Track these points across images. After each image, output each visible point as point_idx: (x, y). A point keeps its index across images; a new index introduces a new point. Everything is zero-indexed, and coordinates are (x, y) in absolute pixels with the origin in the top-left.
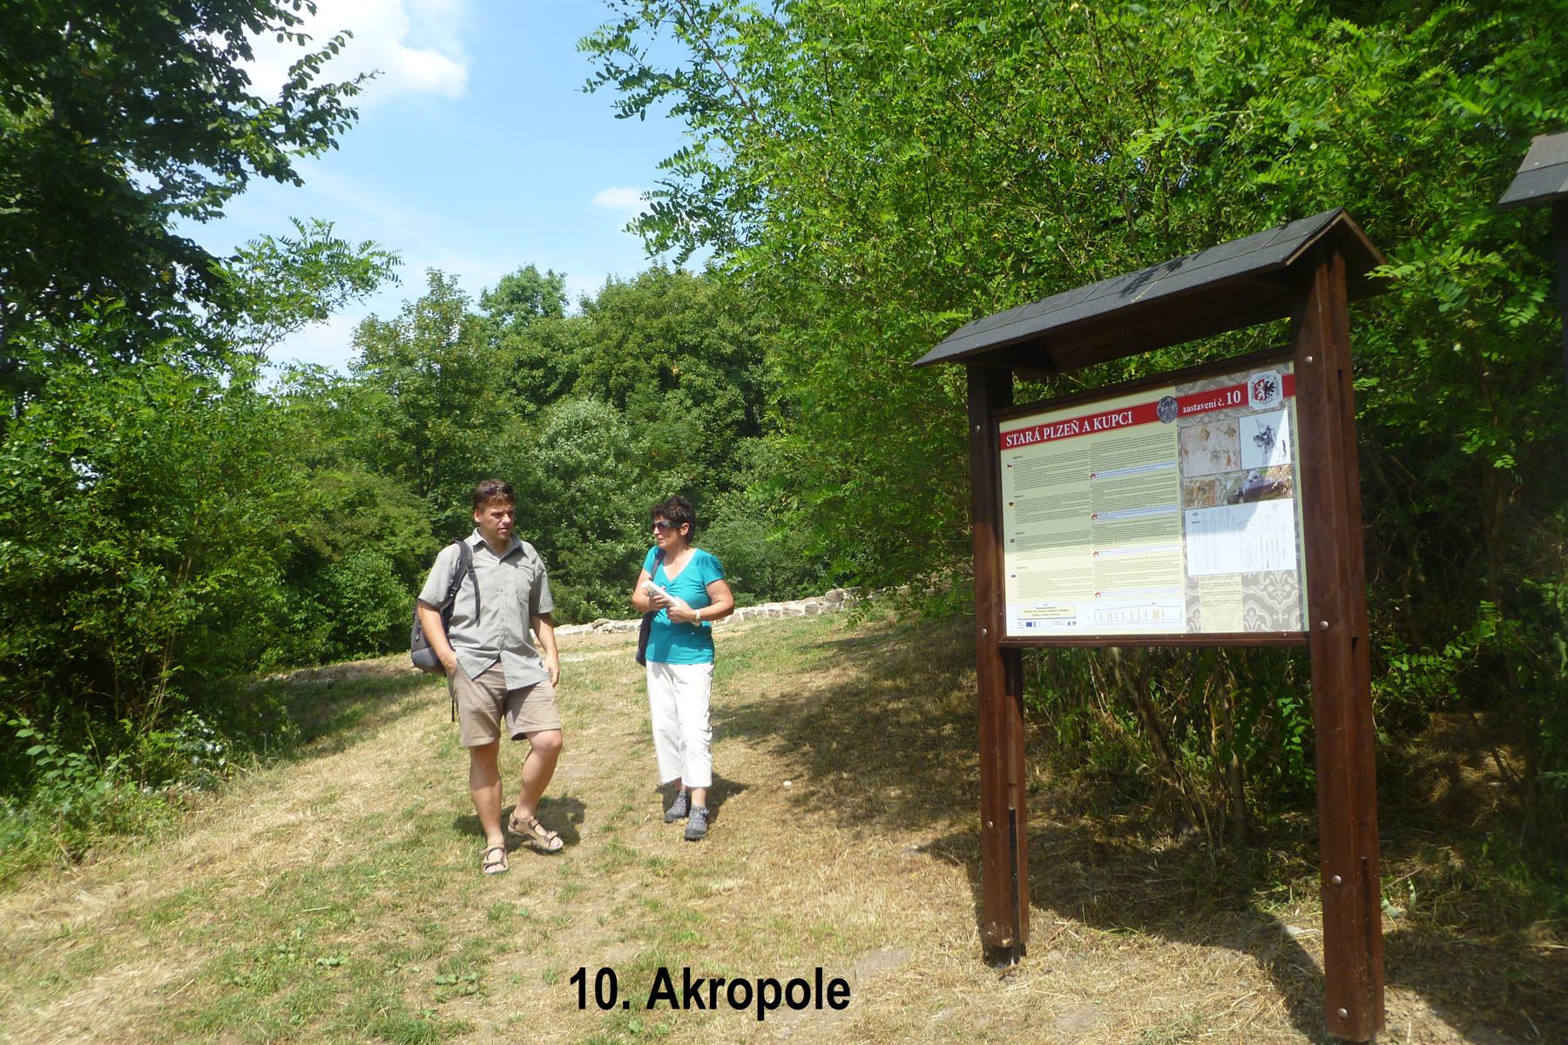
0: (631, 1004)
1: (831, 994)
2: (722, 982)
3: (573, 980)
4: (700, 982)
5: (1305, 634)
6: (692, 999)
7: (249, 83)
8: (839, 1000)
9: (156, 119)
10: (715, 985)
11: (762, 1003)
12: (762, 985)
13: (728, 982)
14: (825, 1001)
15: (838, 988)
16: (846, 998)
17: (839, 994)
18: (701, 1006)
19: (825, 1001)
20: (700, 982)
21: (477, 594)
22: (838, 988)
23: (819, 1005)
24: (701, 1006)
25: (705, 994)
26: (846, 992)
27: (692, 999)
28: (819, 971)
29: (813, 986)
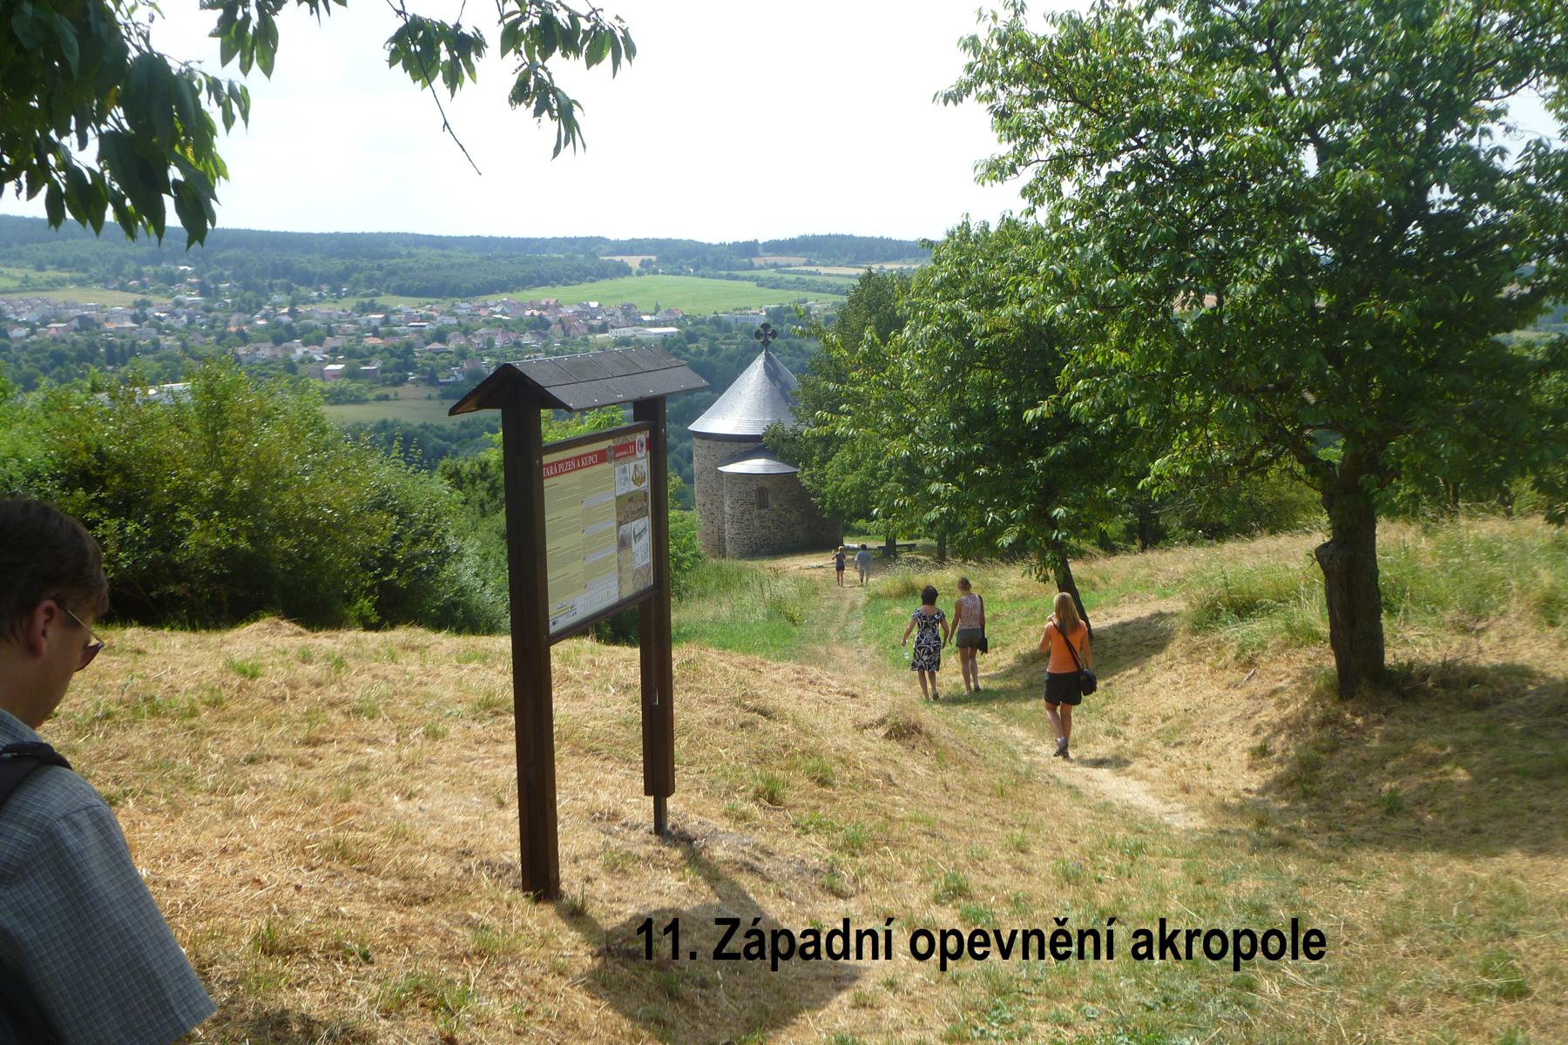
0: (699, 953)
1: (1307, 944)
2: (1198, 932)
3: (666, 931)
4: (1175, 933)
5: (541, 442)
6: (1168, 951)
7: (268, 69)
8: (979, 951)
9: (1333, 62)
10: (1190, 936)
11: (945, 954)
12: (1237, 935)
13: (1204, 933)
14: (1047, 950)
15: (1314, 939)
16: (1322, 949)
17: (979, 945)
18: (1177, 956)
19: (1047, 950)
20: (1175, 933)
21: (620, 570)
22: (1314, 939)
23: (1295, 956)
24: (1177, 956)
25: (1181, 941)
26: (1322, 943)
27: (1168, 951)
28: (1295, 922)
29: (1288, 935)
